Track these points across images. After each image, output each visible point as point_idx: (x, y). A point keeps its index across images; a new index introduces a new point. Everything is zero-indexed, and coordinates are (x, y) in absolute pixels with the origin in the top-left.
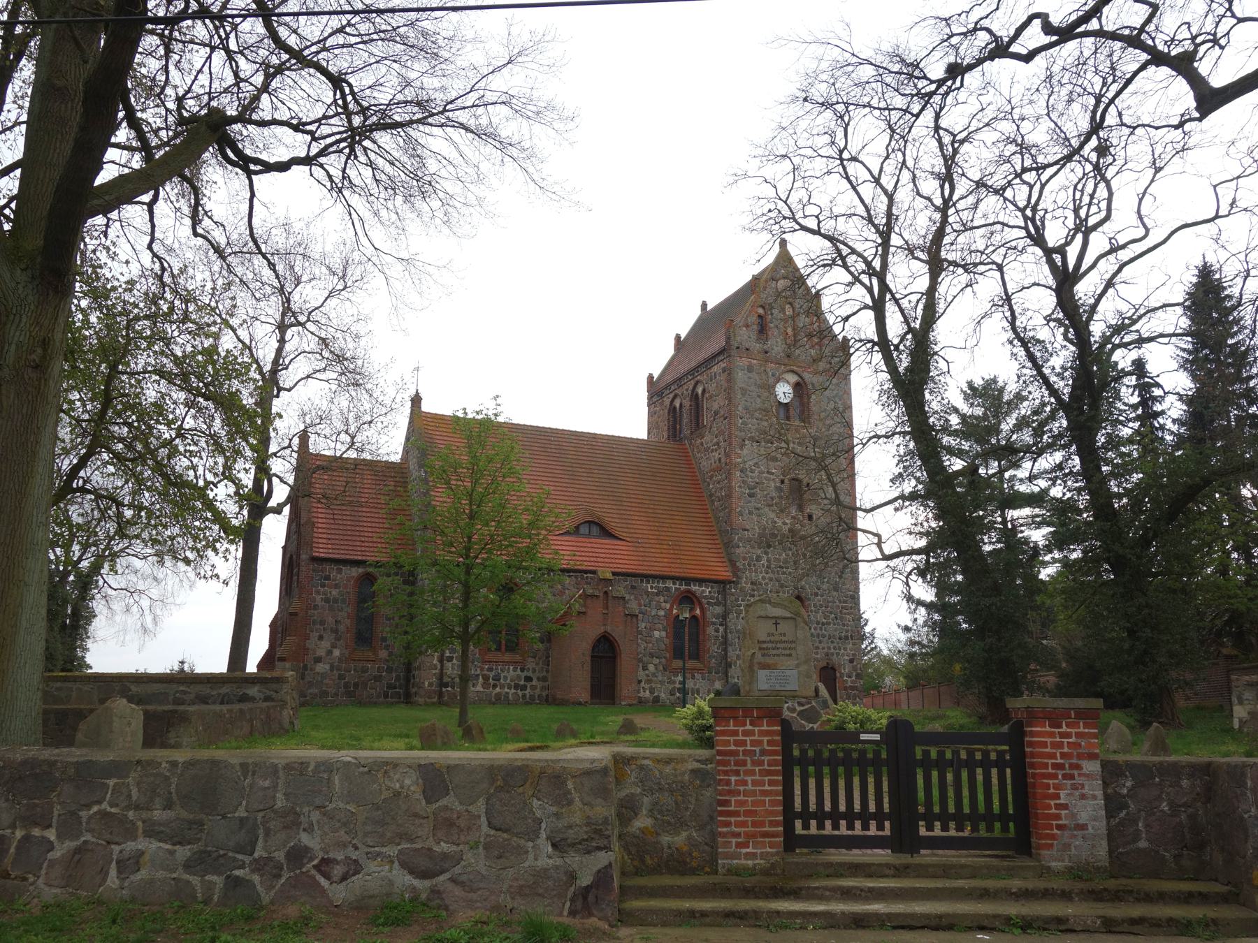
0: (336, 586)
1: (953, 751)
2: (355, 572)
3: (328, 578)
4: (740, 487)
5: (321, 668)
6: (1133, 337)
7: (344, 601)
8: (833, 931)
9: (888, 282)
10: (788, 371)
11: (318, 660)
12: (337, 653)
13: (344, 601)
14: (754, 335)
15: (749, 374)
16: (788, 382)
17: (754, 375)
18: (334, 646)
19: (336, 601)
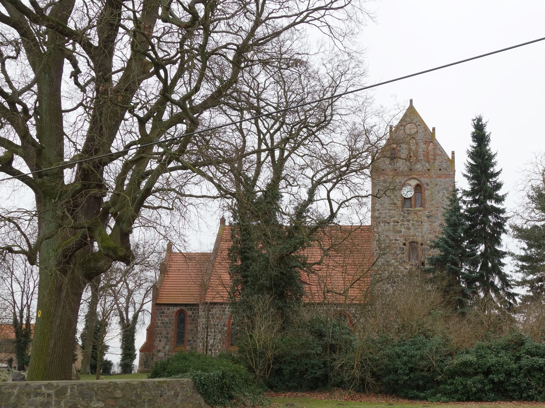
0: (167, 316)
3: (163, 313)
5: (161, 354)
10: (410, 179)
11: (159, 351)
13: (170, 323)
16: (411, 185)
19: (167, 323)
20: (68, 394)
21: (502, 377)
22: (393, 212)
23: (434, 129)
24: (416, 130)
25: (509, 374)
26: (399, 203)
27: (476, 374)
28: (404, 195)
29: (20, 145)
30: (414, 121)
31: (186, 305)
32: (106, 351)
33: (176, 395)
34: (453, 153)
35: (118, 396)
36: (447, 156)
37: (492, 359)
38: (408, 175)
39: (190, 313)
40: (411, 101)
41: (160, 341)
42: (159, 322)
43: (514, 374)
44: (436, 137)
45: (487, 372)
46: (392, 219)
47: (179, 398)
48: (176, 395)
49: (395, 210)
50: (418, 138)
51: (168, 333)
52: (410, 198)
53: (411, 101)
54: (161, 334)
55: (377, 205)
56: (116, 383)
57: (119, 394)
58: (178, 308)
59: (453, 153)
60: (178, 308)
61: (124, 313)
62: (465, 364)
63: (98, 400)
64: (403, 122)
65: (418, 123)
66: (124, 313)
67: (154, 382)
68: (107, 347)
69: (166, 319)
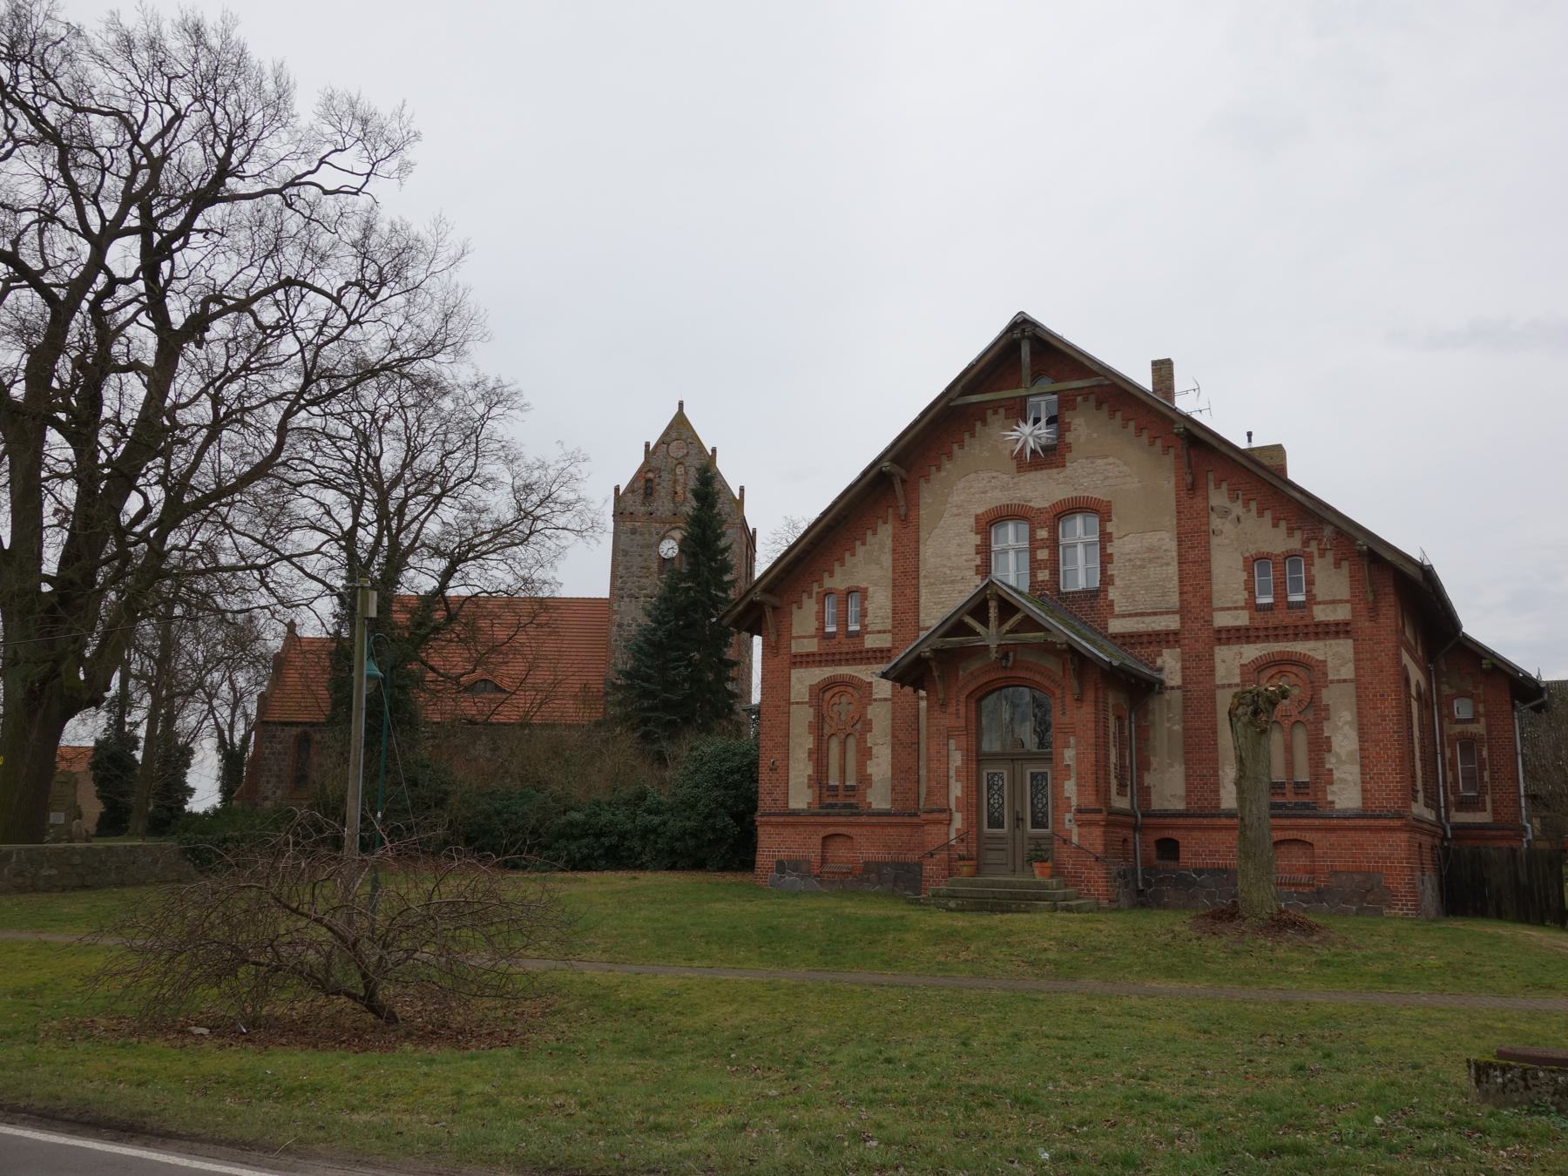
0: (280, 743)
1: (837, 786)
2: (295, 731)
3: (274, 736)
4: (616, 640)
5: (268, 804)
6: (326, 518)
7: (285, 753)
8: (791, 755)
9: (89, 245)
10: (673, 529)
11: (266, 798)
12: (279, 792)
13: (285, 753)
14: (639, 499)
15: (633, 537)
16: (674, 539)
17: (638, 537)
18: (278, 788)
19: (279, 753)
20: (14, 860)
21: (614, 840)
22: (644, 580)
23: (714, 450)
24: (685, 451)
25: (623, 836)
26: (655, 567)
27: (582, 837)
28: (662, 555)
29: (177, 327)
30: (684, 437)
31: (313, 725)
32: (191, 796)
33: (155, 862)
34: (742, 489)
35: (76, 862)
36: (733, 495)
37: (606, 817)
38: (671, 523)
39: (318, 737)
40: (681, 404)
41: (268, 782)
42: (267, 751)
43: (628, 836)
44: (718, 465)
45: (599, 835)
46: (643, 592)
47: (159, 865)
48: (155, 862)
49: (647, 577)
50: (687, 464)
51: (281, 770)
52: (673, 559)
53: (681, 404)
54: (270, 770)
55: (620, 569)
56: (74, 848)
57: (77, 860)
58: (299, 729)
59: (742, 489)
60: (299, 729)
61: (227, 733)
62: (571, 824)
63: (51, 867)
64: (665, 440)
65: (689, 440)
66: (227, 733)
67: (125, 847)
68: (191, 791)
69: (279, 747)
